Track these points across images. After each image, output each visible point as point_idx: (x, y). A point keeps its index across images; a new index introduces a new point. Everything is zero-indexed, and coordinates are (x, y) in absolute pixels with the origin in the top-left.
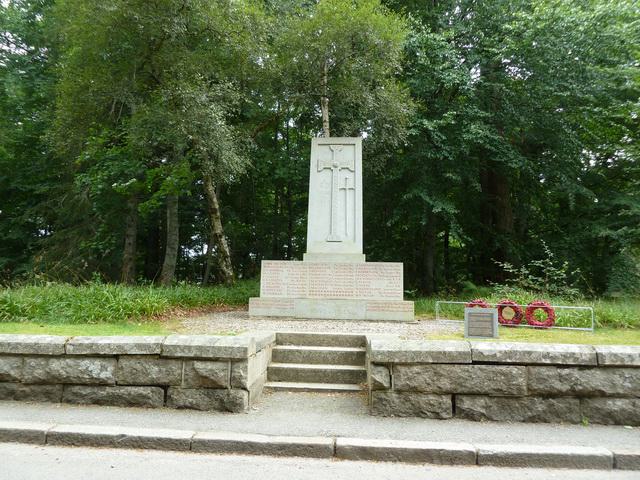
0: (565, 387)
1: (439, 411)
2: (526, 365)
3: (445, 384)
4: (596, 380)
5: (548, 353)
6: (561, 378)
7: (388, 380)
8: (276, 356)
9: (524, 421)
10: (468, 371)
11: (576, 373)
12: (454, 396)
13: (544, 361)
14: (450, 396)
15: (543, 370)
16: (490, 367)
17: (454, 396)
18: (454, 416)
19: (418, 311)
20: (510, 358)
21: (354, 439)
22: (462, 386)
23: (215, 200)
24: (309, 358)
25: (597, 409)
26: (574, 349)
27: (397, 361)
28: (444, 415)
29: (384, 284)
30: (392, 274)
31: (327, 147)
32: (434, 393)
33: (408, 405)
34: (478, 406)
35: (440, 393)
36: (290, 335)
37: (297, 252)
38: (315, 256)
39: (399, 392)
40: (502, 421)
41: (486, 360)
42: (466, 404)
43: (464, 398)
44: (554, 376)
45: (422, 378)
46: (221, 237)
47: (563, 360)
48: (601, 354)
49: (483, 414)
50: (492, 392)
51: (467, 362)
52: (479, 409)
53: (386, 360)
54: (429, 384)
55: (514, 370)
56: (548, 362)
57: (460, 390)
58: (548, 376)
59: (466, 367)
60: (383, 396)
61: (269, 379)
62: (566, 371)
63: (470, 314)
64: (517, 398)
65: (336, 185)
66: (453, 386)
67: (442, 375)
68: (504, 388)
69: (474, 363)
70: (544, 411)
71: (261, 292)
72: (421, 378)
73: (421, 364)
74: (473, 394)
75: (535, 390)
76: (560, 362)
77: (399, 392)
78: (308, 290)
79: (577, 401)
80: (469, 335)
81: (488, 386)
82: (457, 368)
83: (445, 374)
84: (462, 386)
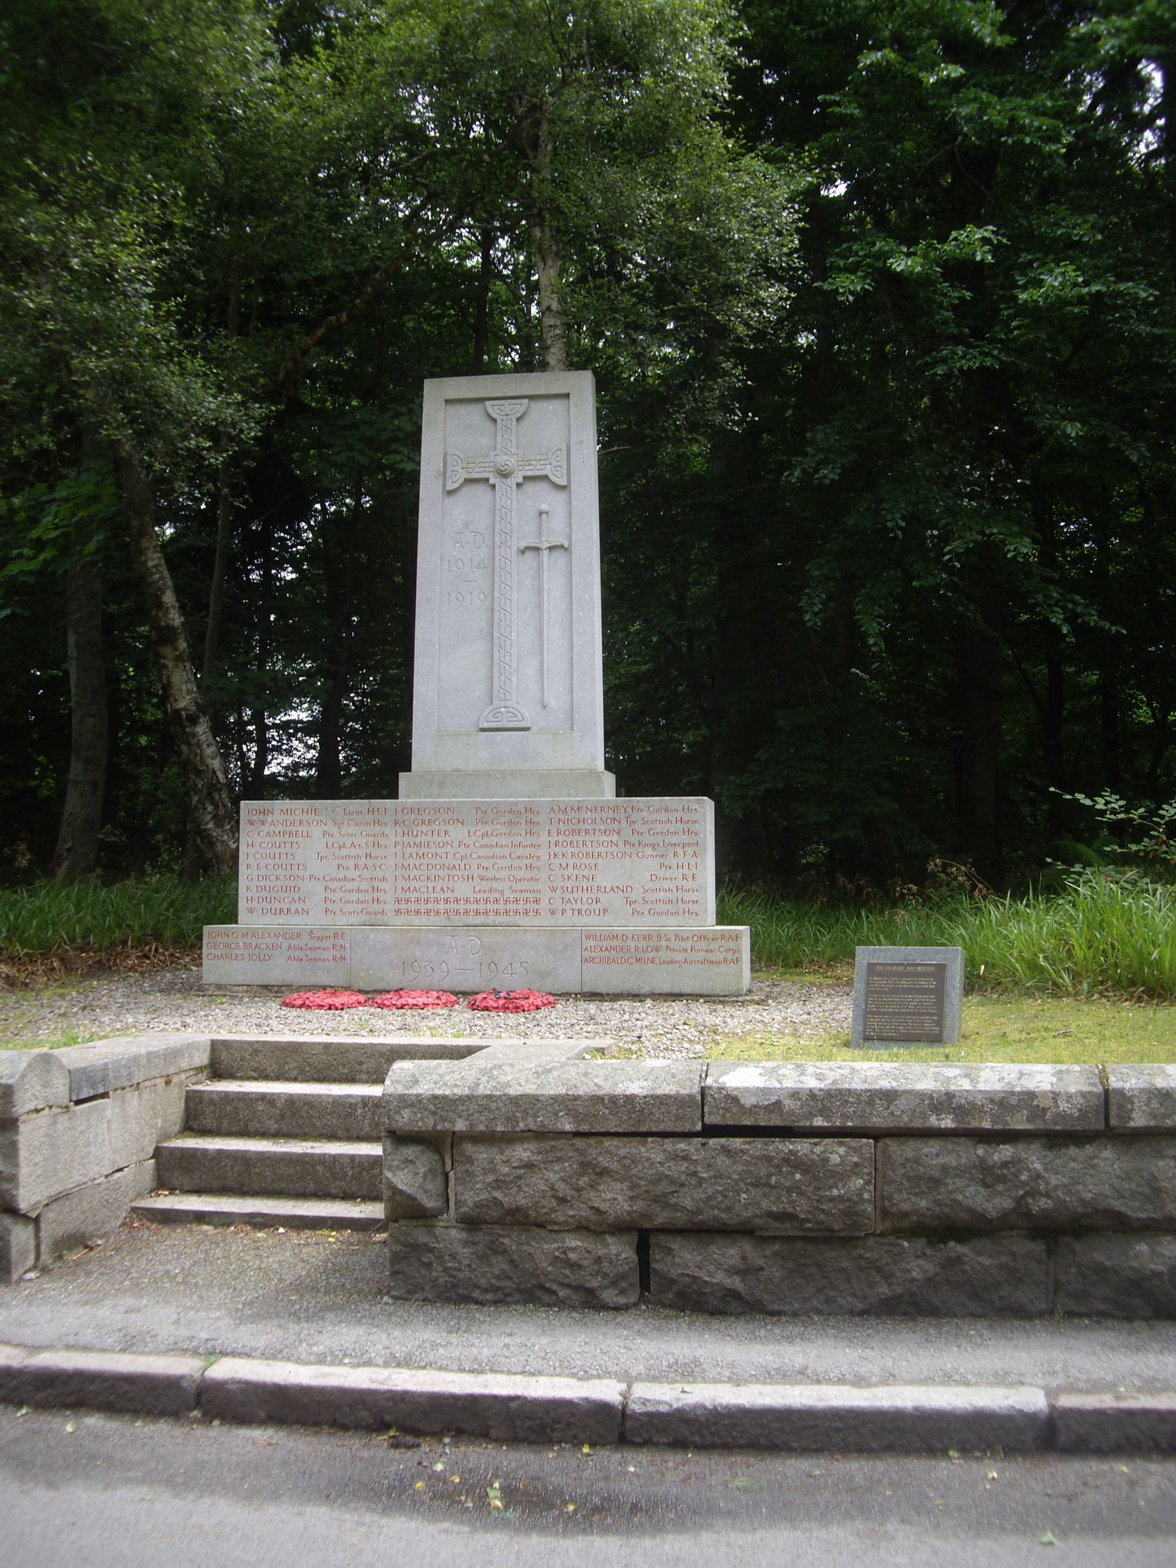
0: (993, 1203)
1: (594, 1283)
2: (877, 1135)
3: (614, 1199)
4: (1100, 1176)
5: (950, 1096)
6: (988, 1176)
7: (435, 1186)
8: (198, 1115)
9: (861, 1313)
10: (685, 1158)
11: (1035, 1159)
12: (644, 1238)
13: (933, 1121)
14: (634, 1237)
15: (930, 1148)
16: (757, 1146)
17: (644, 1238)
18: (642, 1299)
19: (766, 957)
20: (824, 1112)
21: (489, 1377)
22: (666, 1205)
23: (169, 598)
24: (296, 1119)
25: (1101, 1271)
26: (1040, 1077)
27: (460, 1126)
28: (610, 1296)
29: (642, 870)
30: (689, 827)
31: (476, 408)
32: (581, 1228)
33: (499, 1265)
34: (715, 1265)
35: (597, 1227)
36: (256, 1048)
37: (408, 768)
38: (441, 780)
39: (471, 1223)
40: (795, 1314)
41: (747, 1121)
42: (683, 1260)
43: (676, 1244)
44: (961, 1172)
45: (543, 1182)
46: (193, 720)
47: (995, 1118)
48: (1120, 1092)
49: (733, 1294)
50: (759, 1222)
51: (686, 1127)
52: (720, 1277)
53: (427, 1123)
54: (563, 1201)
55: (837, 1153)
56: (947, 1122)
57: (661, 1218)
58: (945, 1169)
59: (682, 1145)
60: (422, 1236)
61: (163, 1183)
62: (1006, 1152)
63: (871, 966)
64: (846, 1241)
65: (512, 549)
66: (639, 1205)
67: (604, 1172)
68: (802, 1207)
69: (710, 1131)
70: (930, 1281)
71: (242, 905)
72: (537, 1183)
73: (540, 1135)
74: (702, 1231)
75: (905, 1215)
76: (986, 1125)
77: (471, 1223)
78: (389, 897)
79: (1039, 1247)
80: (867, 1039)
81: (748, 1204)
82: (653, 1152)
83: (614, 1166)
84: (666, 1205)
